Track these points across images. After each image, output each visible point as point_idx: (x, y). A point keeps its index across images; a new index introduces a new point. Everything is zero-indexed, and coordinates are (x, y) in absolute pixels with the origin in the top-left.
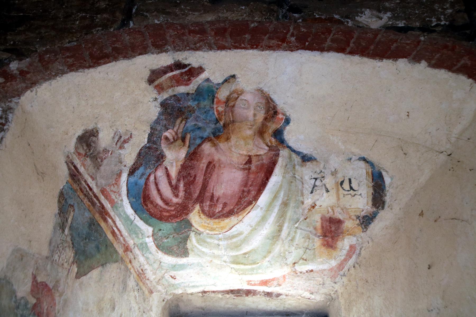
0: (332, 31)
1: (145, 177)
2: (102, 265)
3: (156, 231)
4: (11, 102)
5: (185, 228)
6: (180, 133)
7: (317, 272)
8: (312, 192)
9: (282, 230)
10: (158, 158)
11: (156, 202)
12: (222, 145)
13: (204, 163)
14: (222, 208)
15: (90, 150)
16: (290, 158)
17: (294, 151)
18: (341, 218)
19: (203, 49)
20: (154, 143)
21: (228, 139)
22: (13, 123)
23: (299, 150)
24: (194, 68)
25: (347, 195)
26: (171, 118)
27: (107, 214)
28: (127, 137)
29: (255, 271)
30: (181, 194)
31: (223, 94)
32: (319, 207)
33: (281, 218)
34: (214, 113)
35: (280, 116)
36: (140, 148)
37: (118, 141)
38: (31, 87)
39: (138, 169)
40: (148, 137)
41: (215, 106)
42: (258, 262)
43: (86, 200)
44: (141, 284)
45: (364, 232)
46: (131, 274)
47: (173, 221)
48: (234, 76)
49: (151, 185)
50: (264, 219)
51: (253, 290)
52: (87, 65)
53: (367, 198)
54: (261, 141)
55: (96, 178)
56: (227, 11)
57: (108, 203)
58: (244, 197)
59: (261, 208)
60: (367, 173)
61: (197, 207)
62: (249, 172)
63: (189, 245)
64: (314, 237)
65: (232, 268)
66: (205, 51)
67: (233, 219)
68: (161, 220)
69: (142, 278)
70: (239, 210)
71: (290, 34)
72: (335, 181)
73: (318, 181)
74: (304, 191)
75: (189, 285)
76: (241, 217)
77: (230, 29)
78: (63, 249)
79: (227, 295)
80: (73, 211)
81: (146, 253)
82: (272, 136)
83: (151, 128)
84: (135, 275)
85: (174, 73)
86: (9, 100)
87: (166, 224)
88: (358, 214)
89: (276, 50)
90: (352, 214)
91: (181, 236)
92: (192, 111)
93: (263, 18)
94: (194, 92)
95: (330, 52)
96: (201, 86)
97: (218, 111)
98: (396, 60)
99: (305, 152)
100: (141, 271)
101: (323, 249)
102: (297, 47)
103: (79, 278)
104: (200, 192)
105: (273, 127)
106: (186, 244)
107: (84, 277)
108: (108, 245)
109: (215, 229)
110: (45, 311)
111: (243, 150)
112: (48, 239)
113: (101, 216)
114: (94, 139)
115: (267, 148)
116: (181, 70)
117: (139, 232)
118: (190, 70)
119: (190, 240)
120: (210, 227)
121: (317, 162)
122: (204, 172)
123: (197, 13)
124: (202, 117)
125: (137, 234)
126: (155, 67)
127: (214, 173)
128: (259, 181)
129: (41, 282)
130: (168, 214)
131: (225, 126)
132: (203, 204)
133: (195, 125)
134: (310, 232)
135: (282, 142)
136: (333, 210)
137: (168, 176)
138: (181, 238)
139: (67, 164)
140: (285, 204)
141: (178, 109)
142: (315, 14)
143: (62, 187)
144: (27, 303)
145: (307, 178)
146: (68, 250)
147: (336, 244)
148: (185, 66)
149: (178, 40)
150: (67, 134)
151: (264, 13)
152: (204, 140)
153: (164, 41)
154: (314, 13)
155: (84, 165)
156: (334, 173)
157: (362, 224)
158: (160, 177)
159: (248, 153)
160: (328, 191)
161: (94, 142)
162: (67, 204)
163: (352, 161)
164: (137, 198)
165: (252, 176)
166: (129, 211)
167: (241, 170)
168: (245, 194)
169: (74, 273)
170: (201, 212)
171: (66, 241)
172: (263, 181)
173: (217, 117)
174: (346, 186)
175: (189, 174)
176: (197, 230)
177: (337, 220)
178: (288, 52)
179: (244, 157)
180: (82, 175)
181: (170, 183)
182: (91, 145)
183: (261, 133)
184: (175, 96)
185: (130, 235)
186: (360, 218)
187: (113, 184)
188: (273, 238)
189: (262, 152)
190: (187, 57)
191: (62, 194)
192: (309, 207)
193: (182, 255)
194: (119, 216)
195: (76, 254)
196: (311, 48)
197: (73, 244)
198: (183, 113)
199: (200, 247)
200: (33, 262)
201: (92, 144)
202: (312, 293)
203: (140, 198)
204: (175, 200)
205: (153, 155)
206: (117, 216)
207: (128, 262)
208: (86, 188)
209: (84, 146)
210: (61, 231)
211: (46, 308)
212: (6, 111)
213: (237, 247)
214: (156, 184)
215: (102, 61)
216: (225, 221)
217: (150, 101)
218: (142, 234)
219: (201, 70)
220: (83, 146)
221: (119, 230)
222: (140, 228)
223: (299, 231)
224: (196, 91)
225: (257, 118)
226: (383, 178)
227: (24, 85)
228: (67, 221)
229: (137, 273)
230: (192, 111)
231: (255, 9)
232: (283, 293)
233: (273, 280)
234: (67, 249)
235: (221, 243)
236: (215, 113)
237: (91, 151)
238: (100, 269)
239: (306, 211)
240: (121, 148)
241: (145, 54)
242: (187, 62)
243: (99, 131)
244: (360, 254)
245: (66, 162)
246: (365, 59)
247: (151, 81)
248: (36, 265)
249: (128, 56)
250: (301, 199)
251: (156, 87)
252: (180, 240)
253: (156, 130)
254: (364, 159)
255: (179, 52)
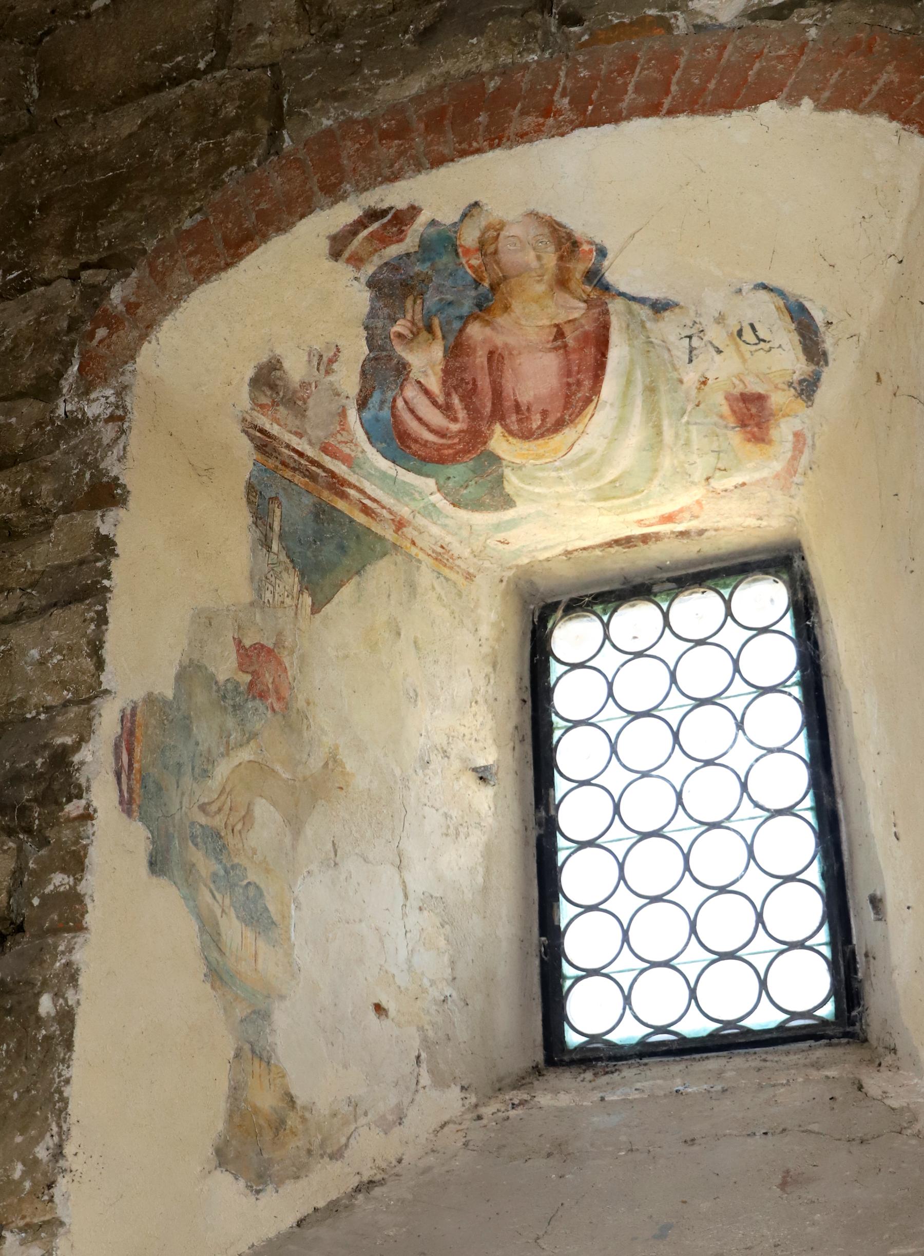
0: (639, 59)
1: (388, 405)
2: (358, 573)
3: (442, 482)
4: (123, 373)
5: (490, 465)
6: (419, 321)
7: (751, 484)
8: (691, 361)
9: (661, 433)
10: (397, 370)
11: (423, 437)
12: (502, 320)
13: (480, 357)
14: (542, 420)
15: (277, 393)
16: (630, 312)
17: (633, 299)
18: (762, 392)
19: (405, 173)
20: (382, 348)
21: (507, 308)
22: (134, 412)
23: (641, 296)
24: (401, 211)
25: (756, 351)
26: (394, 301)
27: (344, 482)
28: (332, 354)
29: (642, 503)
30: (462, 414)
31: (469, 237)
32: (715, 381)
33: (652, 413)
34: (466, 272)
35: (586, 247)
36: (360, 365)
37: (319, 364)
38: (147, 335)
39: (371, 396)
40: (367, 343)
41: (464, 261)
42: (642, 489)
43: (298, 478)
44: (446, 571)
45: (810, 406)
46: (421, 563)
47: (465, 459)
48: (476, 204)
49: (403, 414)
50: (622, 422)
51: (653, 533)
52: (223, 262)
53: (794, 349)
54: (567, 296)
55: (306, 432)
56: (445, 58)
57: (339, 463)
58: (575, 394)
59: (612, 405)
60: (778, 308)
61: (498, 429)
62: (566, 351)
63: (508, 489)
64: (725, 431)
65: (599, 508)
66: (410, 177)
67: (568, 434)
68: (443, 463)
69: (445, 561)
70: (573, 416)
71: (560, 90)
72: (727, 332)
73: (694, 339)
74: (676, 362)
75: (536, 547)
76: (580, 427)
77: (452, 108)
78: (276, 578)
79: (610, 549)
80: (278, 507)
81: (439, 520)
82: (583, 283)
83: (366, 328)
84: (430, 561)
85: (370, 229)
86: (121, 370)
87: (455, 466)
88: (789, 379)
89: (535, 139)
90: (777, 382)
91: (489, 478)
92: (426, 280)
93: (516, 52)
94: (417, 249)
95: (631, 120)
96: (425, 235)
97: (471, 267)
98: (755, 109)
99: (653, 295)
100: (440, 550)
101: (749, 446)
102: (572, 122)
103: (319, 611)
104: (493, 404)
105: (579, 268)
106: (504, 488)
107: (328, 606)
108: (362, 535)
109: (543, 455)
110: (270, 686)
111: (542, 319)
112: (247, 574)
113: (334, 491)
114: (278, 373)
115: (583, 305)
116: (380, 221)
117: (413, 491)
118: (395, 216)
119: (507, 481)
120: (533, 454)
121: (681, 308)
122: (486, 371)
123: (391, 81)
124: (448, 283)
125: (410, 495)
126: (334, 230)
127: (505, 368)
128: (590, 361)
129: (251, 647)
130: (451, 451)
131: (493, 288)
132: (505, 421)
133: (441, 300)
134: (715, 424)
135: (606, 288)
136: (741, 380)
137: (427, 392)
138: (490, 481)
139: (247, 433)
140: (651, 390)
141: (401, 284)
142: (610, 17)
143: (248, 477)
144: (237, 685)
145: (672, 338)
146: (286, 574)
147: (767, 434)
148: (384, 213)
149: (363, 164)
150: (230, 384)
151: (515, 40)
152: (466, 320)
153: (338, 174)
154: (607, 15)
155: (277, 421)
156: (720, 319)
157: (800, 394)
158: (413, 398)
159: (551, 321)
160: (721, 352)
161: (280, 379)
162: (265, 498)
163: (744, 293)
164: (388, 440)
165: (574, 357)
166: (384, 464)
167: (550, 352)
168: (574, 388)
169: (307, 607)
170: (506, 434)
171: (280, 563)
172: (596, 360)
173: (474, 276)
174: (748, 335)
175: (462, 379)
176: (513, 463)
177: (756, 396)
178: (557, 139)
179: (548, 330)
180: (278, 438)
181: (435, 403)
182: (277, 385)
183: (562, 282)
184: (386, 264)
185: (398, 500)
186: (795, 385)
187: (338, 432)
188: (652, 448)
189: (576, 315)
190: (383, 197)
191: (251, 489)
192: (697, 384)
193: (504, 507)
194: (369, 476)
195: (302, 575)
196: (595, 121)
197: (292, 561)
198: (413, 288)
199: (530, 488)
200: (229, 622)
201: (278, 382)
202: (760, 519)
203: (392, 439)
204: (454, 427)
205: (386, 369)
206: (364, 478)
207: (409, 545)
208: (291, 457)
209: (266, 391)
210: (265, 550)
211: (271, 680)
212: (121, 394)
213: (595, 473)
214: (412, 411)
215: (243, 249)
216: (555, 439)
217: (347, 286)
218: (420, 493)
219: (414, 211)
220: (263, 391)
221: (374, 500)
222: (412, 485)
223: (693, 429)
224: (419, 246)
225: (545, 261)
226: (809, 313)
227: (136, 333)
228: (271, 528)
229: (434, 555)
230: (425, 280)
231: (497, 38)
232: (708, 528)
233: (681, 510)
234: (285, 575)
235: (562, 474)
236: (469, 271)
237: (281, 394)
238: (356, 579)
239: (694, 392)
240: (328, 372)
241: (310, 213)
242: (385, 206)
243: (281, 360)
244: (814, 445)
245: (243, 431)
246: (700, 119)
247: (336, 255)
248: (236, 624)
249: (282, 227)
250: (675, 375)
251: (348, 261)
252: (489, 485)
253: (376, 328)
254: (764, 287)
255: (365, 193)
